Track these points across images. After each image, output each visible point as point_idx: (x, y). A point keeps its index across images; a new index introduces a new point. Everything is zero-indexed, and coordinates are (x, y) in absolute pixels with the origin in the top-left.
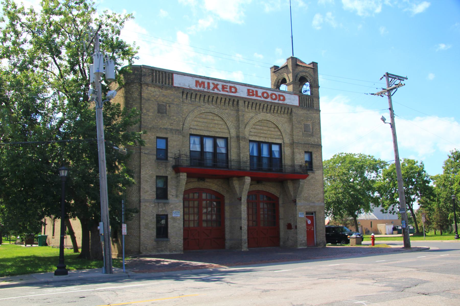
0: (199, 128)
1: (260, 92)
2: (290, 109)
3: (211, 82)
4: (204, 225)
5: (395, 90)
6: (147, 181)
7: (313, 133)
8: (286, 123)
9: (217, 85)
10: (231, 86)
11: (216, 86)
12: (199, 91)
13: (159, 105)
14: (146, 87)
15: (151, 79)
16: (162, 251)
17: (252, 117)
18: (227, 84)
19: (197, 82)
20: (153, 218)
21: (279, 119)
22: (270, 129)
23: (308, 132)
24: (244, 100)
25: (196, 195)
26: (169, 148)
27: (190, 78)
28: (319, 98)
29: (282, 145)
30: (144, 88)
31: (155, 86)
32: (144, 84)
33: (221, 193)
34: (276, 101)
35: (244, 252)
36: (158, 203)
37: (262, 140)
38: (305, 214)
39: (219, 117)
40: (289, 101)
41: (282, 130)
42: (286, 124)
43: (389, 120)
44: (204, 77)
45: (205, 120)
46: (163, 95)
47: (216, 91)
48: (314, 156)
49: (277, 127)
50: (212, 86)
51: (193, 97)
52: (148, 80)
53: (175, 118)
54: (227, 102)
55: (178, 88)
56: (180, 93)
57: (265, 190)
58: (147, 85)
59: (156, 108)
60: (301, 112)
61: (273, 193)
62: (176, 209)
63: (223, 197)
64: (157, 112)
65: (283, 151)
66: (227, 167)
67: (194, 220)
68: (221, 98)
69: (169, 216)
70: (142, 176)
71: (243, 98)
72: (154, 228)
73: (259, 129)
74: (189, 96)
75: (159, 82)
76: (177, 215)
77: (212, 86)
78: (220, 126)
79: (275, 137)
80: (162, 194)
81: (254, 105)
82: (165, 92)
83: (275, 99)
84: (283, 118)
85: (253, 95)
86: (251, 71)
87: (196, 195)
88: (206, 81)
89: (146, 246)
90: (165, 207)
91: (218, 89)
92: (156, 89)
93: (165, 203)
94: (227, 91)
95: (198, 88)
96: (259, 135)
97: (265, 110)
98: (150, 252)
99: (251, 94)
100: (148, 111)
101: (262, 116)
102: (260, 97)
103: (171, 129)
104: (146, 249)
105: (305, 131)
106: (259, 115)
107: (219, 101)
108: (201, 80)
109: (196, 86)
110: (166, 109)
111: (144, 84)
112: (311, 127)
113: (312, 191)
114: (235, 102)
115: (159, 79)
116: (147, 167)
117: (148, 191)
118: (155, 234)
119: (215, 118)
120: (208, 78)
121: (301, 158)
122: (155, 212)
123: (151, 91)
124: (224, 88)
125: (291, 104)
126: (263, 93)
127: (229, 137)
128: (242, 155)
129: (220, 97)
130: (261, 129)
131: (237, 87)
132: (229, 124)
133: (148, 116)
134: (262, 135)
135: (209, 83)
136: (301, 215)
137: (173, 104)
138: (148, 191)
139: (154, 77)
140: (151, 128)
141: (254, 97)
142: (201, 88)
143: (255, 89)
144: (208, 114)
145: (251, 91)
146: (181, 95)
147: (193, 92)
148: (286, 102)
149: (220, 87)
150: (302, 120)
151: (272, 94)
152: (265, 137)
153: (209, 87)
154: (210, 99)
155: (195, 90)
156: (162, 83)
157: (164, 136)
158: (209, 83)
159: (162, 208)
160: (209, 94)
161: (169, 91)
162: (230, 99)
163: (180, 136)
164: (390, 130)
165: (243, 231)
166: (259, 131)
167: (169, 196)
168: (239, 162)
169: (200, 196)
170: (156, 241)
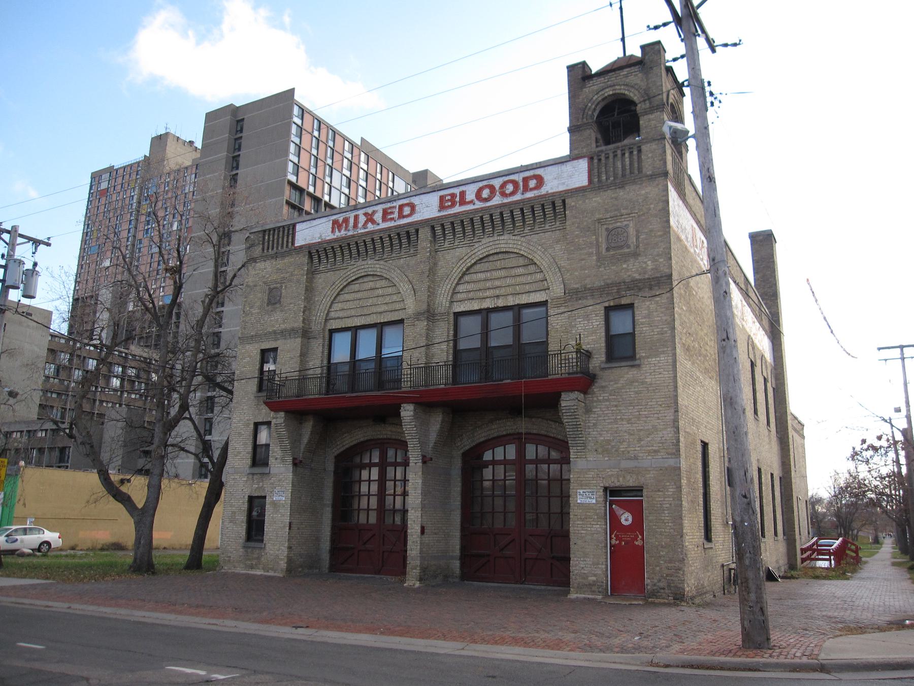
0: (345, 315)
2: (558, 203)
8: (558, 242)
17: (456, 256)
21: (535, 238)
23: (621, 247)
24: (431, 224)
25: (511, 452)
31: (264, 258)
34: (518, 197)
35: (411, 589)
37: (487, 304)
40: (556, 182)
42: (557, 247)
44: (532, 164)
45: (359, 295)
47: (370, 227)
54: (395, 242)
55: (301, 247)
60: (596, 200)
62: (279, 485)
63: (465, 455)
67: (368, 510)
68: (381, 238)
69: (268, 500)
80: (259, 458)
81: (458, 229)
82: (280, 263)
83: (513, 193)
85: (453, 205)
87: (511, 452)
89: (229, 555)
91: (366, 223)
94: (392, 219)
95: (338, 234)
96: (481, 294)
97: (489, 229)
104: (229, 561)
105: (608, 249)
107: (378, 246)
112: (632, 231)
113: (629, 421)
117: (239, 453)
122: (248, 492)
125: (561, 188)
134: (488, 293)
136: (586, 498)
137: (290, 281)
138: (239, 453)
141: (458, 209)
143: (457, 191)
145: (447, 198)
150: (599, 221)
151: (503, 186)
152: (498, 297)
154: (362, 249)
155: (335, 240)
159: (258, 483)
160: (355, 239)
161: (287, 260)
167: (272, 461)
170: (244, 547)
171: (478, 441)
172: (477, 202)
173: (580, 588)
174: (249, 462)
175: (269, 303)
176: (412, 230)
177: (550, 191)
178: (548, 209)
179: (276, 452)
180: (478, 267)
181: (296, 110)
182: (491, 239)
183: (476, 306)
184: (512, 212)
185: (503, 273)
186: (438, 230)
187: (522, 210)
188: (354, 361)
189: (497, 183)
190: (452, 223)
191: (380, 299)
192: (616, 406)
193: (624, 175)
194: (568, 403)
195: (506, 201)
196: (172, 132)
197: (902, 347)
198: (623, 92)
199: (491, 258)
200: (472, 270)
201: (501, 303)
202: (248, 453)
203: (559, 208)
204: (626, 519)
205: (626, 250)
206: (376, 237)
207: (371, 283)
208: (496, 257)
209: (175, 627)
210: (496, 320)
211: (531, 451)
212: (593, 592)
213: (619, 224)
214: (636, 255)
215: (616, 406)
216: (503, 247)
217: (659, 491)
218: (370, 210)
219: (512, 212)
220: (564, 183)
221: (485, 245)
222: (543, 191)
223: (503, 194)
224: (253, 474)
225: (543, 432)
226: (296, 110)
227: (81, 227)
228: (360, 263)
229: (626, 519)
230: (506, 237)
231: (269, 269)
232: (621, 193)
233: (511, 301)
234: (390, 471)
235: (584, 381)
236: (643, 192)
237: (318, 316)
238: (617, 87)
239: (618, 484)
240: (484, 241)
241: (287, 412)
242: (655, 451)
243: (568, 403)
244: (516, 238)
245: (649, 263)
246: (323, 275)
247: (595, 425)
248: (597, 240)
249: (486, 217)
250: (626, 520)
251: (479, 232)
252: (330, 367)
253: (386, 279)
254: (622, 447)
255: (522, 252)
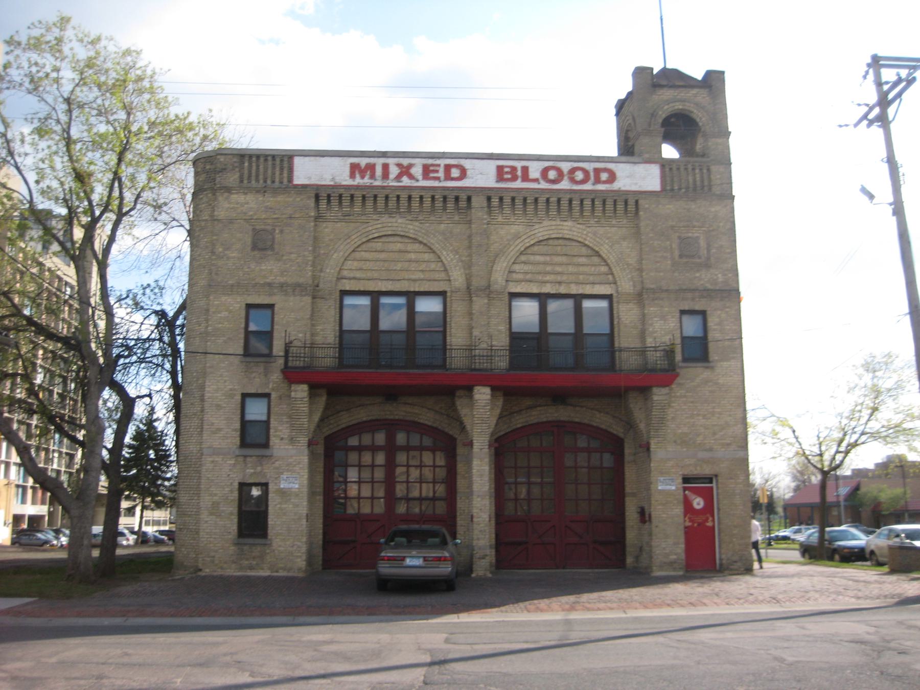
0: (363, 276)
1: (535, 170)
2: (631, 202)
3: (391, 161)
4: (401, 509)
5: (898, 100)
6: (219, 407)
7: (708, 259)
8: (624, 239)
9: (410, 166)
10: (455, 164)
11: (405, 171)
12: (358, 187)
13: (256, 232)
14: (226, 194)
15: (237, 175)
16: (251, 568)
17: (512, 231)
18: (438, 162)
19: (354, 168)
20: (231, 491)
21: (601, 231)
22: (576, 260)
23: (693, 257)
24: (488, 194)
25: (380, 438)
26: (276, 327)
27: (336, 161)
28: (729, 164)
29: (615, 300)
30: (220, 198)
31: (247, 190)
32: (221, 188)
33: (446, 430)
34: (588, 186)
36: (245, 456)
37: (548, 289)
38: (680, 481)
39: (421, 242)
41: (612, 259)
42: (625, 244)
43: (885, 194)
44: (591, 156)
45: (383, 256)
46: (266, 207)
47: (406, 181)
48: (712, 322)
49: (597, 252)
50: (394, 171)
51: (346, 202)
52: (232, 179)
53: (293, 256)
55: (304, 186)
56: (309, 198)
57: (577, 420)
58: (228, 190)
59: (249, 240)
60: (669, 207)
61: (603, 427)
62: (288, 470)
63: (455, 439)
64: (249, 248)
65: (615, 315)
66: (444, 366)
68: (421, 197)
70: (207, 395)
71: (482, 189)
72: (231, 514)
73: (539, 263)
74: (335, 202)
75: (257, 180)
76: (291, 485)
77: (394, 171)
78: (423, 266)
79: (591, 278)
80: (253, 438)
82: (270, 200)
83: (583, 182)
84: (614, 229)
85: (514, 178)
86: (568, 118)
87: (380, 438)
88: (379, 162)
89: (212, 554)
90: (261, 465)
91: (411, 177)
92: (250, 198)
93: (263, 456)
94: (438, 179)
95: (358, 181)
96: (540, 277)
98: (222, 568)
99: (509, 176)
100: (228, 249)
101: (546, 228)
102: (536, 180)
103: (282, 286)
104: (213, 562)
105: (681, 256)
106: (537, 226)
108: (362, 163)
109: (352, 176)
110: (273, 239)
111: (221, 188)
112: (702, 243)
113: (704, 417)
114: (460, 201)
115: (257, 176)
116: (221, 376)
117: (220, 430)
118: (234, 528)
119: (410, 247)
120: (384, 154)
121: (665, 328)
122: (237, 478)
123: (237, 203)
124: (427, 171)
126: (545, 172)
127: (448, 289)
128: (476, 333)
129: (416, 195)
130: (545, 263)
131: (467, 164)
132: (448, 257)
133: (228, 258)
134: (548, 278)
135: (386, 167)
136: (666, 485)
138: (220, 430)
139: (246, 172)
140: (232, 286)
141: (518, 184)
142: (367, 181)
144: (391, 239)
145: (507, 170)
146: (312, 203)
147: (342, 191)
148: (618, 185)
149: (417, 171)
150: (672, 227)
151: (573, 171)
152: (560, 283)
153: (385, 175)
156: (265, 181)
157: (266, 302)
158: (386, 167)
160: (387, 192)
161: (280, 198)
162: (445, 198)
163: (304, 298)
164: (892, 222)
165: (475, 526)
166: (540, 268)
167: (274, 441)
168: (470, 349)
169: (391, 438)
171: (515, 427)
172: (542, 181)
173: (661, 567)
174: (237, 441)
175: (255, 247)
176: (463, 196)
177: (623, 189)
178: (620, 207)
179: (279, 431)
180: (536, 248)
182: (554, 223)
183: (535, 289)
184: (582, 201)
185: (564, 259)
186: (495, 201)
187: (593, 201)
189: (566, 167)
190: (513, 199)
191: (414, 264)
192: (692, 402)
193: (695, 189)
194: (660, 398)
195: (575, 187)
198: (692, 109)
199: (551, 242)
200: (529, 251)
201: (563, 290)
202: (235, 430)
203: (631, 207)
204: (698, 503)
205: (698, 260)
206: (416, 195)
207: (399, 245)
208: (556, 242)
209: (337, 623)
211: (401, 438)
212: (675, 569)
213: (690, 235)
214: (707, 265)
215: (692, 402)
216: (567, 233)
217: (731, 478)
218: (405, 162)
219: (582, 201)
220: (636, 184)
222: (616, 186)
223: (573, 180)
224: (245, 456)
225: (586, 421)
228: (385, 218)
229: (698, 503)
230: (569, 223)
231: (253, 205)
232: (693, 206)
233: (574, 290)
234: (401, 458)
235: (666, 375)
236: (713, 210)
237: (330, 272)
238: (687, 104)
239: (695, 472)
240: (546, 223)
241: (494, 389)
242: (728, 444)
243: (660, 398)
244: (581, 226)
245: (720, 275)
246: (330, 225)
247: (673, 418)
248: (671, 245)
249: (553, 199)
250: (698, 504)
251: (542, 213)
253: (421, 242)
254: (699, 439)
255: (587, 242)
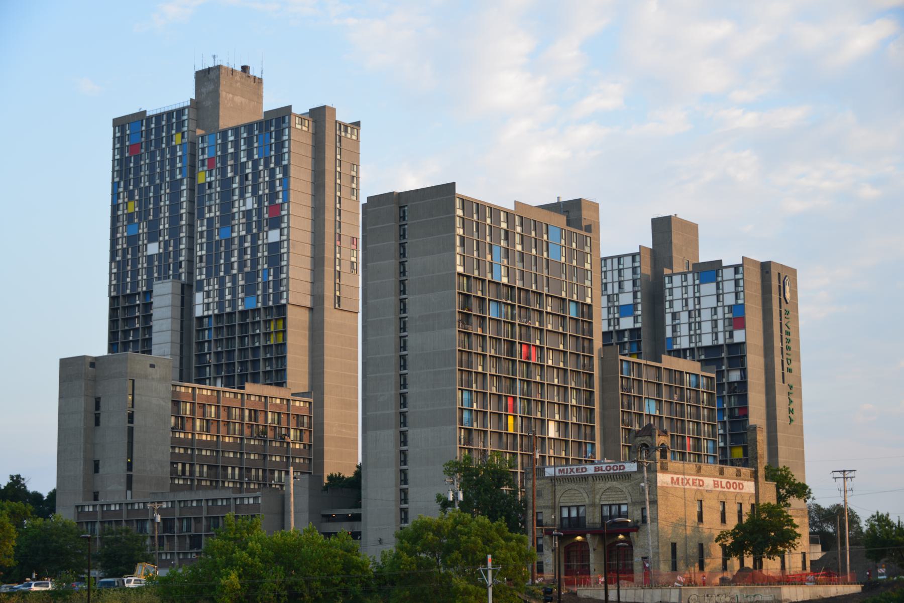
17: (601, 485)
24: (592, 475)
179: (545, 548)
181: (458, 203)
188: (569, 517)
196: (225, 64)
197: (844, 471)
210: (614, 508)
221: (609, 484)
226: (458, 203)
227: (110, 196)
252: (562, 519)
